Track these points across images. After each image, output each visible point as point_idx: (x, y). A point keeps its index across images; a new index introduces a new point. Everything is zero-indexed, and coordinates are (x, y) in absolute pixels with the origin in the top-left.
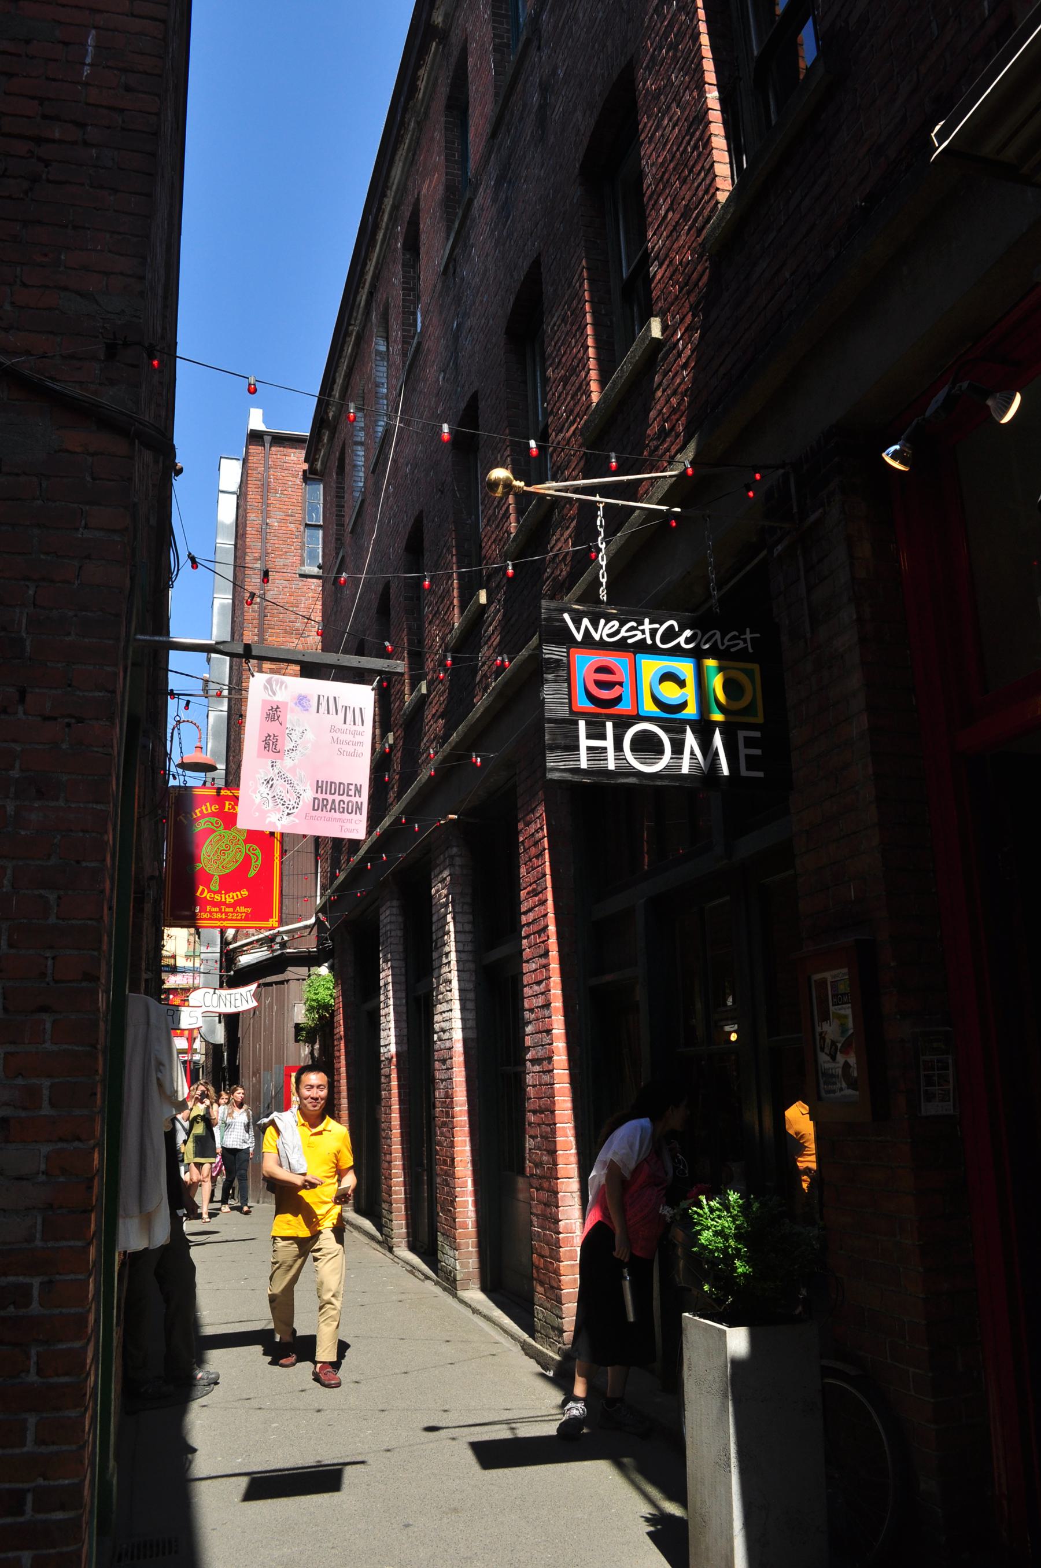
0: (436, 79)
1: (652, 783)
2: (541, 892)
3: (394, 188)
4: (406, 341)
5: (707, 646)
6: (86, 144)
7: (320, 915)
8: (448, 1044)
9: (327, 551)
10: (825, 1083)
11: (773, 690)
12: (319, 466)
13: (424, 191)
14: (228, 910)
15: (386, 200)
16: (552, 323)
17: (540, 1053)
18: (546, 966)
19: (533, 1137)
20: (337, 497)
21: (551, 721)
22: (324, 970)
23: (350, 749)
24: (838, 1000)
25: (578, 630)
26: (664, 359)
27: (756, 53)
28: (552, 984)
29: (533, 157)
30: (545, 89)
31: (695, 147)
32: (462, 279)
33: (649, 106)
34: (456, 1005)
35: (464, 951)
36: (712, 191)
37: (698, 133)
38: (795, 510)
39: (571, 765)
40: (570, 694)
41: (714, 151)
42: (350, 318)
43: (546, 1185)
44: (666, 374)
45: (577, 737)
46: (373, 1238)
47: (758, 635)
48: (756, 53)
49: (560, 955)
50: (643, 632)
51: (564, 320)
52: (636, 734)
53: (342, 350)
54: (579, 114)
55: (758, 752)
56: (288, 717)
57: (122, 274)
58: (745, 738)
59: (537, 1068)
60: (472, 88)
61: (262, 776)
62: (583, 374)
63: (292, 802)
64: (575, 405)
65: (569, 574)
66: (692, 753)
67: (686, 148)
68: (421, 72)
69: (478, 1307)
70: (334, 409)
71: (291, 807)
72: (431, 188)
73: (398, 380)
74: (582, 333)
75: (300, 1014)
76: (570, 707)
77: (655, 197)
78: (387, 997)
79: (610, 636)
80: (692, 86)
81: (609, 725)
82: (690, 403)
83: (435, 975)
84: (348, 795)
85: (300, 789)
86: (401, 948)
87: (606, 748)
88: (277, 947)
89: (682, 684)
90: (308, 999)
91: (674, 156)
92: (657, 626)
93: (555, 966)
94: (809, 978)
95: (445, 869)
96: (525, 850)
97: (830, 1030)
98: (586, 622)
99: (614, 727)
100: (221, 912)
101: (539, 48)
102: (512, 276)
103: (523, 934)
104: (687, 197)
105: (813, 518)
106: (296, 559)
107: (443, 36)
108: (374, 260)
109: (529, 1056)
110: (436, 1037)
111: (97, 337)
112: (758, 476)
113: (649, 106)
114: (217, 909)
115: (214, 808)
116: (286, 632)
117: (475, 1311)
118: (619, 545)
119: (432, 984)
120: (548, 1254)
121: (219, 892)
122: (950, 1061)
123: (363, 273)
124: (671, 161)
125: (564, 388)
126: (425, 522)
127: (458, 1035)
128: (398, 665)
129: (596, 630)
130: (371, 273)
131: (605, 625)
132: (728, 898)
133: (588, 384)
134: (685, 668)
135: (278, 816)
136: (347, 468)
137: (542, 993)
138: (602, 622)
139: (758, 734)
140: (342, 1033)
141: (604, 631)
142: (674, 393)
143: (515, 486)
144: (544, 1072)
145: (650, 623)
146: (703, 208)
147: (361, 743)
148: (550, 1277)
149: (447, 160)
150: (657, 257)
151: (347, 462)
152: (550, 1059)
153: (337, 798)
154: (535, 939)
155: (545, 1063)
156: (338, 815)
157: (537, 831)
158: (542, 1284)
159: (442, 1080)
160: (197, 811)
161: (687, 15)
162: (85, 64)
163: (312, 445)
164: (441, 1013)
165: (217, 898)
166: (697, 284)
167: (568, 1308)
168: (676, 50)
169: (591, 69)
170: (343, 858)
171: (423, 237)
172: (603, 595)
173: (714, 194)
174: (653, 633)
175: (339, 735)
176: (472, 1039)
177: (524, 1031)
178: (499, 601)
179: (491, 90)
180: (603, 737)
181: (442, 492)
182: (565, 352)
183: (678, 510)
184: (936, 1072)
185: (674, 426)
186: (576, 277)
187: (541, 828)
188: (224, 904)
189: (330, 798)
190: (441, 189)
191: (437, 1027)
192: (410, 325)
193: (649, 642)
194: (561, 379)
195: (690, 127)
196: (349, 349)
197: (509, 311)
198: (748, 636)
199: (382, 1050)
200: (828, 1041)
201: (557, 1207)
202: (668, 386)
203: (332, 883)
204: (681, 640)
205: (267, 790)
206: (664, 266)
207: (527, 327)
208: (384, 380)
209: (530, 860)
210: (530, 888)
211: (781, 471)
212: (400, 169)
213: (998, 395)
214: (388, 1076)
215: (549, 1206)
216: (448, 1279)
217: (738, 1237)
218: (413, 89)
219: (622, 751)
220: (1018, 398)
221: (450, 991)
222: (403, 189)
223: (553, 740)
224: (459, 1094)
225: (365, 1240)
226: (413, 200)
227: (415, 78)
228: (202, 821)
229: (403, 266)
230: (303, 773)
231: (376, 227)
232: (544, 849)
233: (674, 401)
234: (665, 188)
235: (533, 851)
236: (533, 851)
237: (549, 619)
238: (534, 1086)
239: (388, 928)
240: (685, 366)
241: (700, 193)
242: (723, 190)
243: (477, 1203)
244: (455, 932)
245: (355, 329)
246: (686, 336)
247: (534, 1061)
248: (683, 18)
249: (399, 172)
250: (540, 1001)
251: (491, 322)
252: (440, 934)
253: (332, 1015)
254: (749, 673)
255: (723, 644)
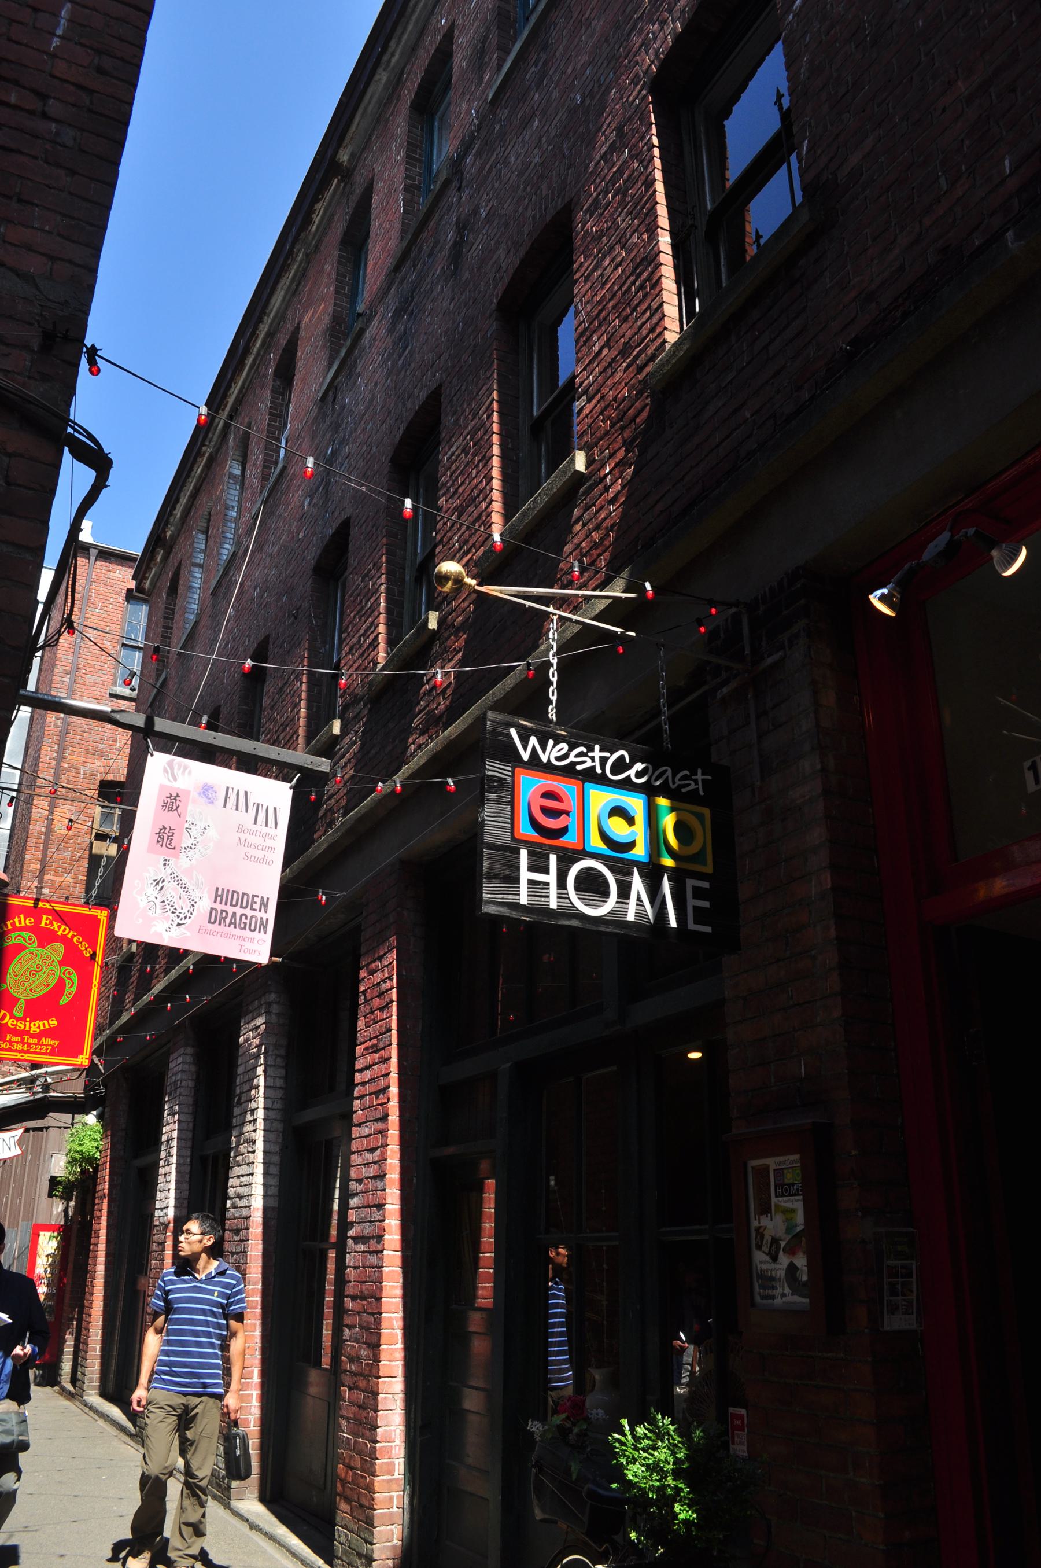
0: (333, 215)
1: (594, 928)
2: (383, 1048)
3: (272, 315)
4: (269, 462)
5: (658, 783)
6: (45, 116)
7: (94, 1057)
8: (244, 1213)
9: (146, 672)
10: (761, 1287)
11: (723, 836)
12: (147, 585)
13: (306, 320)
14: (31, 1041)
15: (261, 326)
16: (450, 454)
17: (368, 1230)
18: (383, 1132)
19: (350, 1327)
20: (165, 618)
21: (490, 846)
22: (91, 1119)
23: (260, 854)
24: (785, 1190)
25: (525, 748)
26: (587, 493)
27: (709, 207)
28: (389, 1153)
29: (442, 291)
30: (462, 227)
31: (642, 287)
32: (343, 407)
33: (587, 246)
34: (259, 1169)
35: (272, 1109)
36: (659, 330)
37: (645, 274)
38: (747, 652)
39: (510, 899)
40: (512, 819)
41: (664, 292)
42: (204, 439)
43: (362, 1384)
44: (587, 508)
45: (517, 868)
46: (122, 1429)
47: (709, 778)
48: (709, 207)
49: (400, 1120)
50: (593, 759)
51: (465, 450)
52: (580, 872)
53: (191, 470)
54: (501, 252)
55: (706, 904)
56: (189, 808)
57: (70, 262)
58: (694, 887)
59: (361, 1247)
60: (375, 225)
61: (152, 874)
62: (484, 505)
63: (185, 911)
64: (470, 536)
65: (448, 709)
66: (639, 899)
67: (630, 288)
68: (318, 206)
69: (258, 1522)
70: (173, 528)
71: (182, 916)
72: (315, 318)
73: (254, 502)
74: (486, 464)
75: (59, 1166)
76: (512, 833)
77: (588, 333)
78: (169, 1154)
79: (558, 759)
80: (642, 229)
81: (553, 858)
82: (616, 539)
83: (235, 1133)
84: (252, 909)
85: (195, 895)
86: (190, 1100)
87: (548, 884)
88: (39, 1089)
89: (631, 821)
90: (70, 1150)
91: (614, 295)
92: (607, 754)
93: (394, 1132)
94: (745, 1165)
95: (260, 1015)
96: (366, 1001)
97: (773, 1225)
98: (533, 741)
99: (558, 860)
100: (22, 1042)
101: (459, 189)
102: (404, 405)
103: (356, 1094)
104: (628, 335)
105: (770, 661)
106: (108, 678)
107: (346, 174)
108: (240, 384)
109: (351, 1233)
110: (229, 1203)
111: (31, 324)
112: (713, 611)
113: (587, 246)
114: (18, 1039)
115: (29, 922)
116: (87, 752)
117: (253, 1527)
118: (519, 679)
119: (230, 1142)
120: (359, 1466)
121: (23, 1019)
122: (914, 1267)
123: (225, 395)
124: (610, 300)
125: (459, 517)
126: (271, 646)
127: (257, 1203)
128: (322, 763)
129: (544, 751)
130: (234, 397)
131: (554, 747)
132: (614, 1068)
133: (489, 515)
134: (636, 804)
135: (167, 925)
136: (181, 589)
137: (375, 1163)
138: (551, 742)
139: (706, 885)
140: (106, 1191)
141: (552, 753)
142: (597, 528)
143: (466, 584)
144: (370, 1252)
145: (601, 751)
146: (647, 346)
147: (272, 849)
148: (359, 1494)
149: (337, 292)
150: (585, 392)
151: (181, 582)
152: (380, 1238)
153: (239, 911)
154: (371, 1100)
155: (373, 1242)
156: (237, 932)
157: (384, 981)
158: (348, 1501)
159: (233, 1253)
160: (9, 923)
161: (641, 162)
162: (55, 35)
163: (142, 566)
164: (239, 1177)
165: (21, 1025)
166: (633, 420)
167: (380, 1532)
168: (625, 194)
169: (520, 210)
170: (129, 997)
171: (300, 365)
172: (552, 713)
173: (661, 333)
174: (603, 761)
175: (247, 836)
176: (273, 1209)
177: (348, 1204)
178: (356, 732)
179: (398, 226)
180: (546, 871)
181: (296, 618)
182: (463, 483)
183: (633, 634)
184: (900, 1280)
185: (595, 560)
186: (484, 408)
187: (390, 978)
188: (28, 1033)
189: (231, 910)
190: (327, 320)
191: (231, 1192)
192: (273, 450)
193: (599, 771)
194: (456, 509)
195: (636, 269)
196: (198, 470)
197: (397, 439)
198: (699, 777)
199: (157, 1213)
200: (767, 1238)
201: (376, 1411)
202: (590, 520)
203: (111, 1023)
204: (632, 772)
205: (155, 893)
206: (594, 402)
207: (416, 455)
208: (235, 504)
209: (372, 1012)
210: (366, 1044)
211: (734, 610)
212: (281, 297)
213: (1004, 545)
214: (162, 1244)
215: (365, 1409)
216: (219, 1486)
217: (677, 1474)
218: (308, 221)
219: (566, 889)
220: (1024, 553)
221: (253, 1152)
222: (281, 317)
223: (492, 868)
224: (253, 1270)
225: (112, 1431)
226: (291, 329)
227: (311, 211)
228: (13, 935)
229: (273, 391)
230: (200, 877)
231: (247, 351)
232: (392, 1001)
233: (596, 536)
234: (600, 325)
235: (377, 1002)
236: (377, 1002)
237: (494, 732)
238: (355, 1268)
239: (179, 1077)
240: (612, 501)
241: (644, 332)
242: (671, 331)
243: (264, 1398)
244: (265, 1087)
245: (208, 451)
246: (616, 472)
247: (357, 1239)
248: (636, 165)
249: (279, 301)
250: (372, 1171)
251: (374, 449)
252: (246, 1087)
253: (96, 1170)
254: (700, 817)
255: (674, 783)
